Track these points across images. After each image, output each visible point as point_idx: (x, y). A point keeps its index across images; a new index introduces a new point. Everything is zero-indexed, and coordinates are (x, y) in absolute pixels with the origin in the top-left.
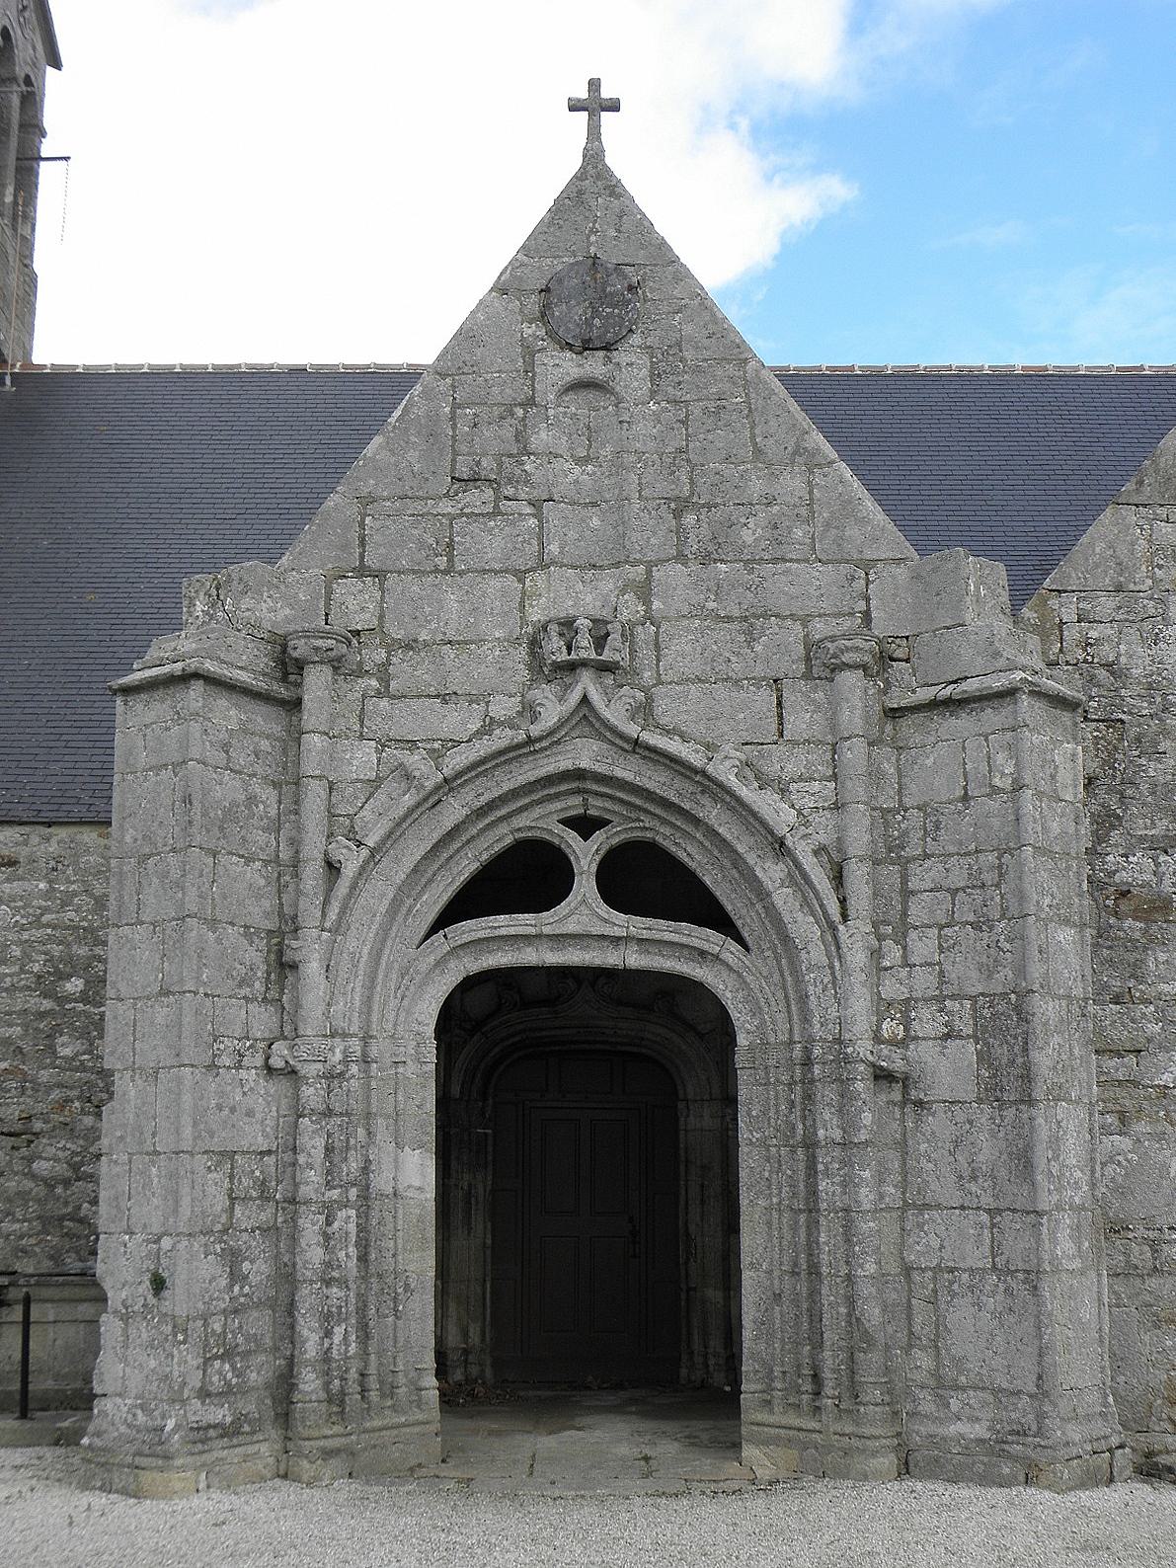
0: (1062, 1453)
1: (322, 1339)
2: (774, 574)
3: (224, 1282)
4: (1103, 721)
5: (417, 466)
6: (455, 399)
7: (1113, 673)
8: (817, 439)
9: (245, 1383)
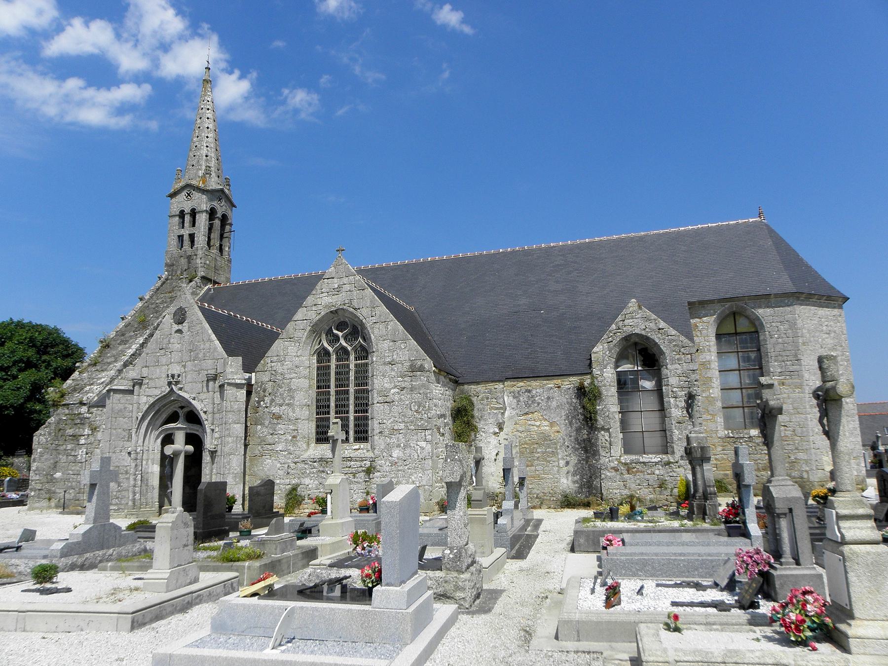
3: (117, 487)
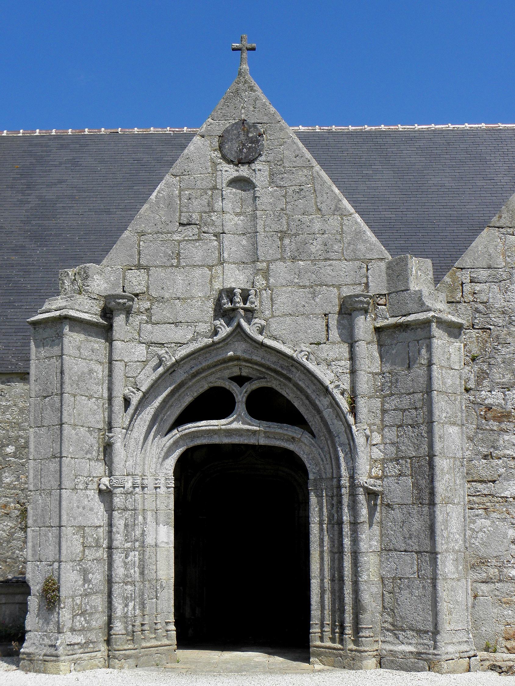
0: (444, 657)
1: (124, 608)
2: (325, 266)
3: (81, 582)
4: (481, 329)
5: (164, 218)
6: (180, 187)
7: (486, 307)
8: (346, 203)
9: (91, 626)
